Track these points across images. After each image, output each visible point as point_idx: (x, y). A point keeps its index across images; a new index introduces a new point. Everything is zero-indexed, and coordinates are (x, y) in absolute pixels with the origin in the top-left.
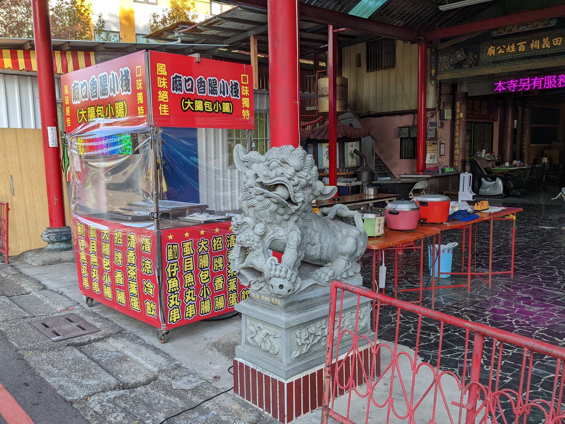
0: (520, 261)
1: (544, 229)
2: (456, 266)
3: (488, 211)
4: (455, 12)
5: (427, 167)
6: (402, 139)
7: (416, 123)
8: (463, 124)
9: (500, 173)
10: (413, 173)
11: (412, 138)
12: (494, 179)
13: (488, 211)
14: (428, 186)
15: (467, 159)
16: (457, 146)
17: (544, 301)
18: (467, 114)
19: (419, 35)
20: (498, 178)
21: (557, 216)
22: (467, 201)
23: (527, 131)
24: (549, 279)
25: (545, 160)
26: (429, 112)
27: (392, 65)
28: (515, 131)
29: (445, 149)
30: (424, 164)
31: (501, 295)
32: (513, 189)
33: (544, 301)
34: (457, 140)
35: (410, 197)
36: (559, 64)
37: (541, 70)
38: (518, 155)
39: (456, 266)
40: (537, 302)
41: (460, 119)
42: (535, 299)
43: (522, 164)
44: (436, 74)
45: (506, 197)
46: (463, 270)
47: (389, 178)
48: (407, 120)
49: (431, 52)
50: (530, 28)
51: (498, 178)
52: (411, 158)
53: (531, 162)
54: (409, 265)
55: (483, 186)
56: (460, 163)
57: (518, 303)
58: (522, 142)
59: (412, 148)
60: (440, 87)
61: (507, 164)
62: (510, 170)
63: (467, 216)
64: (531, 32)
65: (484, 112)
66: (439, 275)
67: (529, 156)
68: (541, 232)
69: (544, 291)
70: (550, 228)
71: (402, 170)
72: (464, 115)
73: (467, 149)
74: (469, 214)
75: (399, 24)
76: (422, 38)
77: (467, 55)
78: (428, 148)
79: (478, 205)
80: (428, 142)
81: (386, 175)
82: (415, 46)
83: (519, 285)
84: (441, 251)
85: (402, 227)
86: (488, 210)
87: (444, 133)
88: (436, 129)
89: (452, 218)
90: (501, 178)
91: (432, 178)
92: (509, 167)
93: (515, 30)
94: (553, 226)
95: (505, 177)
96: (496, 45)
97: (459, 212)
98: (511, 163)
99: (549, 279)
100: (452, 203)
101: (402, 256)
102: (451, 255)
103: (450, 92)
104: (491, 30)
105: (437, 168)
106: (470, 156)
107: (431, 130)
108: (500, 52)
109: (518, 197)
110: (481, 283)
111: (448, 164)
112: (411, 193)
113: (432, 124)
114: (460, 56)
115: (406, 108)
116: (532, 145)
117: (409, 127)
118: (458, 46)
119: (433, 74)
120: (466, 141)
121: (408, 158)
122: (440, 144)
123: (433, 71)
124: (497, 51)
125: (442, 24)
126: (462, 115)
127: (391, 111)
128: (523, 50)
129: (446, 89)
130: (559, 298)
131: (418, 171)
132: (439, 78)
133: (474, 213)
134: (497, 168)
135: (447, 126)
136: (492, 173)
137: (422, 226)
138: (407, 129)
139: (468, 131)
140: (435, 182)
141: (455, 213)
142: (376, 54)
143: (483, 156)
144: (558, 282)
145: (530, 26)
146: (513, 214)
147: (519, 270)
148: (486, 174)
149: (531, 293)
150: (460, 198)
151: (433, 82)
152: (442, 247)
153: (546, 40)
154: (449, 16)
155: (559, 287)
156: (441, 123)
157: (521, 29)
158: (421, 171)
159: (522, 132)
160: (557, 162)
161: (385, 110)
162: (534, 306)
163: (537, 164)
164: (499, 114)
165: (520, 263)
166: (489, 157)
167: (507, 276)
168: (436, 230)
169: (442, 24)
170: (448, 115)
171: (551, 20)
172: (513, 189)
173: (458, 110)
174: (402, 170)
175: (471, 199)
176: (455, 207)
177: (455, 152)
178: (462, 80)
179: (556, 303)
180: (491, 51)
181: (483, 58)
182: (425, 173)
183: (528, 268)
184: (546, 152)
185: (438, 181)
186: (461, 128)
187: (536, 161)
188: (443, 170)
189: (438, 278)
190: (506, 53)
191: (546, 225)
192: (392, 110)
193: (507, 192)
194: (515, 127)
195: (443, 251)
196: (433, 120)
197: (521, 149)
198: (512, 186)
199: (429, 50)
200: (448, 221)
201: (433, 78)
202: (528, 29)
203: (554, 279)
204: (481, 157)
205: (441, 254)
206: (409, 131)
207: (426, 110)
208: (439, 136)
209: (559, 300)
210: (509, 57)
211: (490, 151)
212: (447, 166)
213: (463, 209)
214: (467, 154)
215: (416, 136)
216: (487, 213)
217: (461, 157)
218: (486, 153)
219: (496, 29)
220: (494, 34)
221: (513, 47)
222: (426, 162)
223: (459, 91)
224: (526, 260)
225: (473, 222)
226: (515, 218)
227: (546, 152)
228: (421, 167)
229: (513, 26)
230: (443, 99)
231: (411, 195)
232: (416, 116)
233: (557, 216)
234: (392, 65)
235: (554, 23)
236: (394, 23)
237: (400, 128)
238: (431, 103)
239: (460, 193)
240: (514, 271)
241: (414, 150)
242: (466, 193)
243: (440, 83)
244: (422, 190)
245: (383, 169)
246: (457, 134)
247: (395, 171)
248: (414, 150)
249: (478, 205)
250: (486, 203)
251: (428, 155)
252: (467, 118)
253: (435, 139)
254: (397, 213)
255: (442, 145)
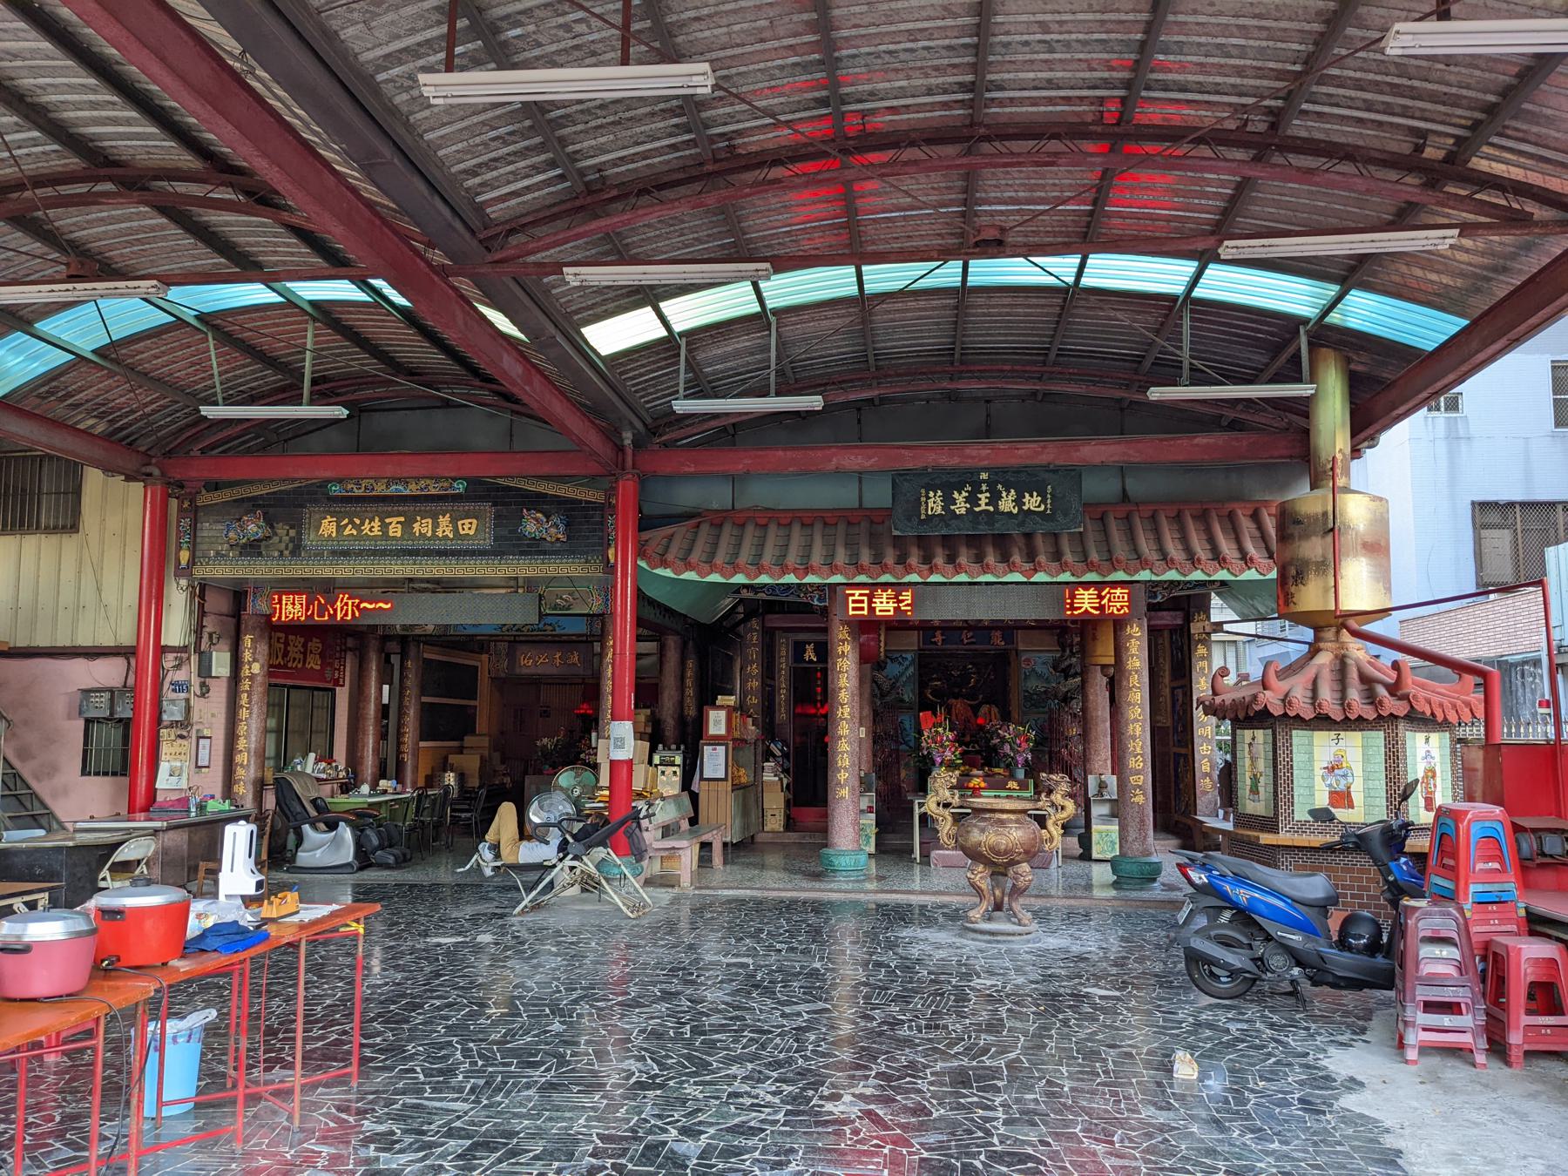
0: (379, 1034)
1: (439, 945)
2: (213, 1075)
3: (295, 919)
4: (245, 425)
5: (160, 798)
6: (88, 721)
7: (131, 681)
8: (259, 690)
9: (347, 812)
10: (116, 817)
11: (120, 720)
12: (332, 826)
13: (295, 919)
14: (156, 852)
15: (269, 776)
16: (242, 744)
17: (423, 1133)
18: (271, 666)
19: (149, 464)
20: (342, 824)
21: (469, 910)
22: (243, 897)
23: (412, 712)
24: (441, 1072)
25: (450, 779)
26: (171, 656)
27: (70, 524)
28: (384, 711)
29: (211, 751)
30: (152, 792)
31: (324, 1140)
32: (377, 849)
33: (423, 1133)
34: (242, 729)
35: (102, 884)
36: (471, 575)
37: (437, 581)
38: (391, 767)
39: (210, 1077)
40: (408, 1139)
41: (252, 677)
42: (405, 1132)
43: (399, 788)
44: (192, 562)
45: (361, 869)
46: (229, 1085)
47: (41, 832)
48: (109, 673)
49: (181, 510)
50: (412, 489)
51: (342, 824)
52: (114, 774)
53: (421, 783)
54: (74, 1091)
55: (305, 845)
56: (250, 787)
57: (363, 1153)
58: (400, 734)
59: (121, 744)
60: (202, 596)
61: (365, 789)
62: (371, 804)
63: (238, 937)
64: (414, 499)
65: (314, 664)
66: (159, 1110)
67: (416, 769)
68: (429, 955)
69: (426, 1107)
70: (453, 940)
71: (84, 805)
72: (262, 667)
73: (271, 751)
74: (245, 931)
75: (93, 426)
76: (156, 472)
77: (272, 527)
78: (165, 749)
79: (271, 903)
80: (164, 732)
81: (34, 821)
82: (137, 487)
83: (371, 1102)
84: (168, 1040)
85: (40, 988)
86: (299, 913)
87: (210, 712)
88: (187, 700)
89: (196, 948)
90: (347, 821)
91: (169, 829)
92: (370, 796)
93: (380, 489)
94: (459, 934)
95: (360, 820)
96: (339, 516)
97: (217, 929)
98: (374, 786)
99: (441, 1072)
100: (197, 906)
101: (57, 1064)
102: (196, 1047)
103: (229, 612)
104: (329, 481)
105: (184, 802)
106: (278, 769)
107: (173, 701)
108: (346, 532)
109: (387, 867)
110: (275, 1113)
111: (218, 790)
112: (105, 873)
113: (178, 687)
114: (253, 528)
115: (107, 640)
116: (422, 744)
117: (111, 691)
118: (252, 504)
119: (184, 562)
120: (266, 731)
121: (105, 774)
122: (198, 738)
123: (185, 556)
124: (340, 529)
125: (213, 447)
126: (256, 668)
127: (59, 644)
128: (399, 534)
129: (217, 603)
130: (459, 1117)
131: (131, 810)
132: (201, 572)
133: (258, 927)
134: (342, 799)
135: (219, 692)
136: (329, 811)
137: (105, 978)
138: (107, 695)
139: (272, 707)
140: (179, 839)
141: (204, 934)
142: (24, 490)
143: (309, 770)
144: (460, 1078)
145: (413, 486)
146: (357, 921)
147: (372, 1059)
148: (313, 813)
149: (398, 1118)
150: (224, 888)
151: (184, 582)
152: (172, 1026)
153: (444, 521)
154: (225, 433)
155: (460, 1090)
156: (203, 685)
157: (394, 489)
158: (142, 810)
159: (401, 713)
160: (474, 782)
161: (42, 641)
162: (401, 1151)
163: (432, 787)
164: (348, 669)
165: (378, 1040)
166: (324, 771)
167: (341, 1081)
168: (145, 987)
169: (213, 447)
170: (221, 664)
171: (454, 479)
172: (377, 849)
173: (247, 656)
174: (84, 805)
175: (251, 890)
176: (207, 916)
177: (238, 758)
178: (259, 585)
179: (450, 1134)
180: (328, 527)
181: (310, 539)
182: (151, 815)
183: (394, 1050)
184: (453, 759)
185: (186, 837)
186: (255, 698)
187: (430, 781)
188: (201, 807)
189: (157, 1120)
190: (360, 537)
191: (444, 935)
192: (63, 641)
193: (364, 859)
194: (385, 700)
195: (175, 1039)
196: (180, 676)
197: (399, 752)
198: (375, 841)
199: (174, 503)
200: (183, 957)
201: (180, 572)
202: (407, 492)
203: (450, 1072)
204: (303, 773)
205: (169, 1048)
206: (112, 699)
207: (161, 650)
208: (195, 717)
209: (458, 1124)
210: (367, 545)
211: (327, 757)
212: (212, 797)
213: (229, 918)
214: (270, 763)
215: (129, 714)
216: (292, 924)
217: (252, 770)
218: (317, 761)
219: (340, 481)
220: (335, 490)
221: (376, 523)
222: (158, 785)
223: (250, 610)
224: (392, 1030)
225: (253, 952)
226: (361, 931)
227: (453, 759)
228: (141, 799)
229: (376, 479)
230: (210, 625)
231: (104, 879)
232: (133, 662)
233: (469, 910)
234: (70, 524)
235: (460, 487)
236: (79, 422)
237: (87, 692)
238: (175, 629)
239: (224, 877)
240: (360, 1065)
241: (125, 752)
242: (238, 871)
243: (203, 587)
244: (139, 862)
245: (29, 805)
246: (244, 714)
247: (64, 810)
248: (125, 752)
249: (271, 903)
250: (292, 897)
251: (164, 768)
252: (270, 674)
253: (185, 724)
254: (26, 949)
255: (202, 742)
